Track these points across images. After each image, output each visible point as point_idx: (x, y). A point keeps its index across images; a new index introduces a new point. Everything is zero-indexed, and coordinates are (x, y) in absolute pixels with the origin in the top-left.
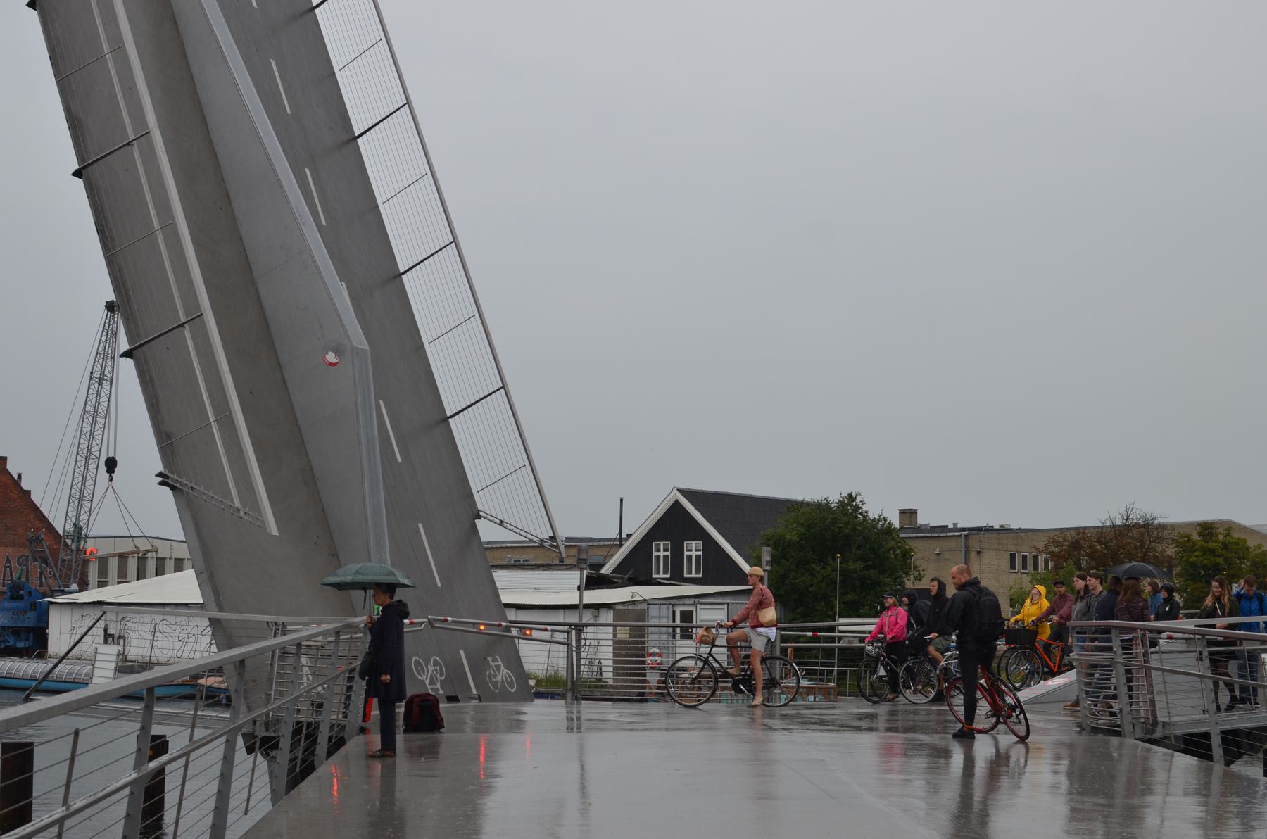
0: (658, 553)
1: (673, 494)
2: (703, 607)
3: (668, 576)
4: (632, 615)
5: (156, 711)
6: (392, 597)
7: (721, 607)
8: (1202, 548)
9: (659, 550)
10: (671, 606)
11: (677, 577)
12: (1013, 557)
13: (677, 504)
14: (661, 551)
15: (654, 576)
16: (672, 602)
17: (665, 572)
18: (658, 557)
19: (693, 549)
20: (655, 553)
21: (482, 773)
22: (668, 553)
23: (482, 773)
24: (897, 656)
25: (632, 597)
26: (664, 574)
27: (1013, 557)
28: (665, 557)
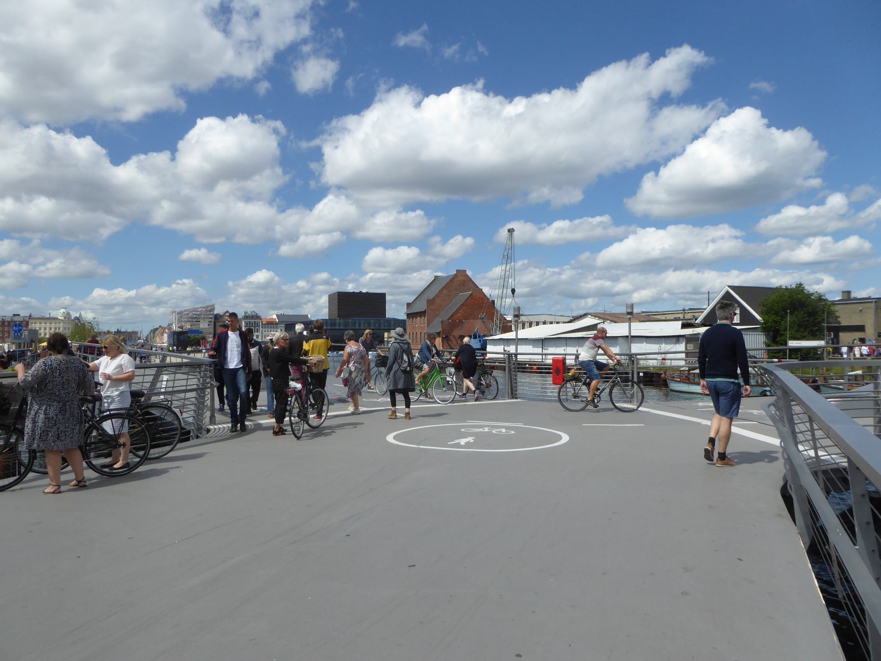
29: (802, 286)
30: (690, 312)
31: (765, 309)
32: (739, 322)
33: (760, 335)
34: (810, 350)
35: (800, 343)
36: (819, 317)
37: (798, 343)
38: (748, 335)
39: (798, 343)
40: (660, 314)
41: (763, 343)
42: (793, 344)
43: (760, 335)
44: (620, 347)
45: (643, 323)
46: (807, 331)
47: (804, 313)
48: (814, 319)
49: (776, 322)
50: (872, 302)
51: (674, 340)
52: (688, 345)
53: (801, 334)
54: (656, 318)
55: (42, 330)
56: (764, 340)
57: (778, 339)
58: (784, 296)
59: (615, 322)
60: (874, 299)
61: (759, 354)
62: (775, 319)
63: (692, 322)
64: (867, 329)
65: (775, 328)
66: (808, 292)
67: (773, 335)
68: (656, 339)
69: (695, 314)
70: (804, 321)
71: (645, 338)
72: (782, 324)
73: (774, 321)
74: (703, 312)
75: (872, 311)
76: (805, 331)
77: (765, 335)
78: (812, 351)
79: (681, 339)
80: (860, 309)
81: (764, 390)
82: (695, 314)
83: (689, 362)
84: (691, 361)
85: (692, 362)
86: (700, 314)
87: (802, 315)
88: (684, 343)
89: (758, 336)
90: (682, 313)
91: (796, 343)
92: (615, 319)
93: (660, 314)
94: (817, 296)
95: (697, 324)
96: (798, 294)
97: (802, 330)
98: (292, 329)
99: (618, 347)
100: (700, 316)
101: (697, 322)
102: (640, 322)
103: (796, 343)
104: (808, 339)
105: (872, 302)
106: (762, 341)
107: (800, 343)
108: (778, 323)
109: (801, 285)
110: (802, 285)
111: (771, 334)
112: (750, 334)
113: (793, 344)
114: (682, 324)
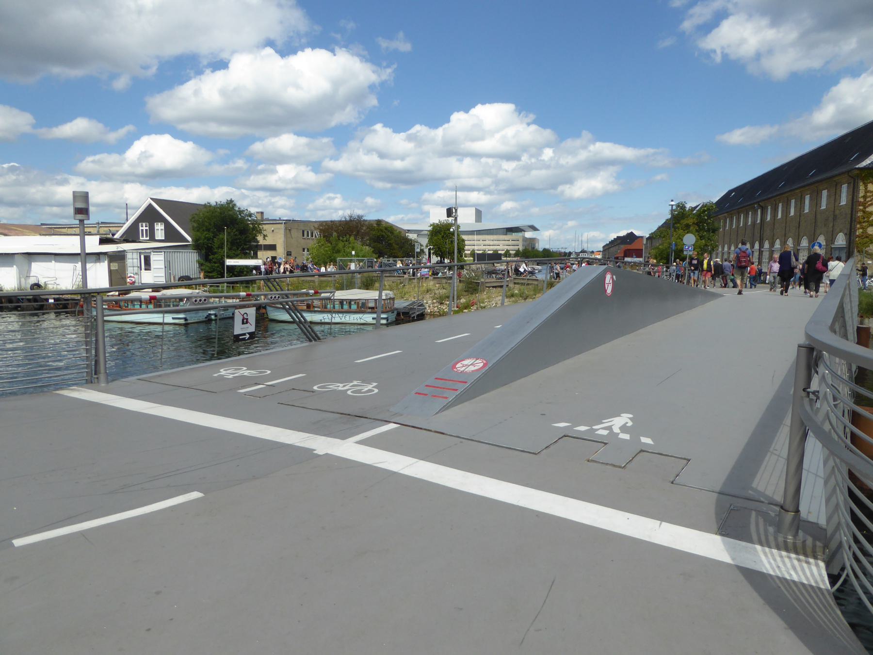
0: (142, 228)
1: (148, 200)
2: (154, 253)
3: (148, 238)
4: (118, 258)
5: (185, 273)
6: (430, 263)
7: (161, 253)
8: (377, 229)
9: (142, 226)
10: (138, 253)
11: (152, 239)
12: (303, 232)
13: (150, 206)
14: (143, 227)
15: (141, 238)
16: (139, 251)
17: (146, 237)
18: (142, 230)
19: (159, 228)
20: (141, 228)
21: (454, 228)
22: (148, 228)
23: (454, 228)
24: (859, 169)
25: (117, 249)
26: (146, 237)
27: (303, 232)
28: (146, 230)
29: (234, 203)
30: (103, 227)
31: (195, 225)
32: (164, 238)
33: (188, 253)
34: (243, 269)
35: (238, 262)
36: (250, 236)
37: (236, 262)
38: (181, 253)
39: (236, 262)
40: (65, 228)
41: (196, 261)
42: (230, 262)
43: (193, 253)
44: (16, 266)
45: (47, 236)
46: (240, 249)
47: (236, 231)
48: (246, 238)
49: (208, 239)
50: (282, 223)
51: (94, 257)
52: (111, 264)
53: (234, 252)
54: (61, 232)
55: (804, 258)
56: (197, 259)
57: (211, 257)
58: (216, 211)
59: (5, 235)
60: (284, 220)
61: (192, 275)
62: (207, 236)
63: (110, 236)
64: (278, 248)
65: (207, 245)
66: (239, 208)
67: (206, 252)
68: (66, 257)
69: (111, 229)
70: (236, 239)
71: (53, 256)
72: (215, 242)
73: (205, 238)
74: (122, 227)
75: (282, 232)
76: (238, 249)
77: (198, 252)
78: (245, 269)
79: (101, 256)
80: (273, 229)
81: (209, 314)
82: (111, 229)
83: (196, 301)
84: (198, 299)
85: (200, 300)
86: (117, 229)
87: (234, 233)
88: (106, 262)
89: (168, 254)
90: (96, 227)
91: (234, 262)
92: (6, 232)
93: (65, 228)
94: (247, 213)
95: (116, 239)
96: (229, 210)
97: (235, 248)
98: (123, 254)
99: (15, 266)
100: (118, 231)
101: (115, 237)
102: (40, 235)
103: (234, 262)
104: (241, 258)
105: (282, 223)
106: (195, 260)
107: (238, 262)
108: (211, 240)
109: (231, 201)
110: (233, 201)
111: (203, 252)
112: (182, 252)
113: (230, 262)
114: (100, 239)
